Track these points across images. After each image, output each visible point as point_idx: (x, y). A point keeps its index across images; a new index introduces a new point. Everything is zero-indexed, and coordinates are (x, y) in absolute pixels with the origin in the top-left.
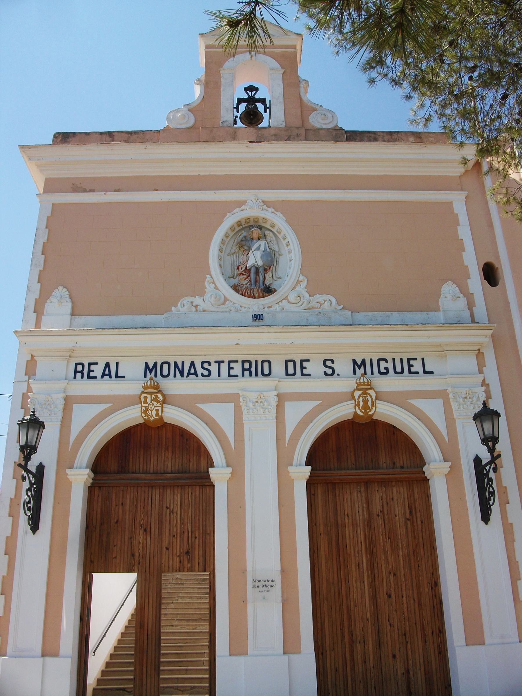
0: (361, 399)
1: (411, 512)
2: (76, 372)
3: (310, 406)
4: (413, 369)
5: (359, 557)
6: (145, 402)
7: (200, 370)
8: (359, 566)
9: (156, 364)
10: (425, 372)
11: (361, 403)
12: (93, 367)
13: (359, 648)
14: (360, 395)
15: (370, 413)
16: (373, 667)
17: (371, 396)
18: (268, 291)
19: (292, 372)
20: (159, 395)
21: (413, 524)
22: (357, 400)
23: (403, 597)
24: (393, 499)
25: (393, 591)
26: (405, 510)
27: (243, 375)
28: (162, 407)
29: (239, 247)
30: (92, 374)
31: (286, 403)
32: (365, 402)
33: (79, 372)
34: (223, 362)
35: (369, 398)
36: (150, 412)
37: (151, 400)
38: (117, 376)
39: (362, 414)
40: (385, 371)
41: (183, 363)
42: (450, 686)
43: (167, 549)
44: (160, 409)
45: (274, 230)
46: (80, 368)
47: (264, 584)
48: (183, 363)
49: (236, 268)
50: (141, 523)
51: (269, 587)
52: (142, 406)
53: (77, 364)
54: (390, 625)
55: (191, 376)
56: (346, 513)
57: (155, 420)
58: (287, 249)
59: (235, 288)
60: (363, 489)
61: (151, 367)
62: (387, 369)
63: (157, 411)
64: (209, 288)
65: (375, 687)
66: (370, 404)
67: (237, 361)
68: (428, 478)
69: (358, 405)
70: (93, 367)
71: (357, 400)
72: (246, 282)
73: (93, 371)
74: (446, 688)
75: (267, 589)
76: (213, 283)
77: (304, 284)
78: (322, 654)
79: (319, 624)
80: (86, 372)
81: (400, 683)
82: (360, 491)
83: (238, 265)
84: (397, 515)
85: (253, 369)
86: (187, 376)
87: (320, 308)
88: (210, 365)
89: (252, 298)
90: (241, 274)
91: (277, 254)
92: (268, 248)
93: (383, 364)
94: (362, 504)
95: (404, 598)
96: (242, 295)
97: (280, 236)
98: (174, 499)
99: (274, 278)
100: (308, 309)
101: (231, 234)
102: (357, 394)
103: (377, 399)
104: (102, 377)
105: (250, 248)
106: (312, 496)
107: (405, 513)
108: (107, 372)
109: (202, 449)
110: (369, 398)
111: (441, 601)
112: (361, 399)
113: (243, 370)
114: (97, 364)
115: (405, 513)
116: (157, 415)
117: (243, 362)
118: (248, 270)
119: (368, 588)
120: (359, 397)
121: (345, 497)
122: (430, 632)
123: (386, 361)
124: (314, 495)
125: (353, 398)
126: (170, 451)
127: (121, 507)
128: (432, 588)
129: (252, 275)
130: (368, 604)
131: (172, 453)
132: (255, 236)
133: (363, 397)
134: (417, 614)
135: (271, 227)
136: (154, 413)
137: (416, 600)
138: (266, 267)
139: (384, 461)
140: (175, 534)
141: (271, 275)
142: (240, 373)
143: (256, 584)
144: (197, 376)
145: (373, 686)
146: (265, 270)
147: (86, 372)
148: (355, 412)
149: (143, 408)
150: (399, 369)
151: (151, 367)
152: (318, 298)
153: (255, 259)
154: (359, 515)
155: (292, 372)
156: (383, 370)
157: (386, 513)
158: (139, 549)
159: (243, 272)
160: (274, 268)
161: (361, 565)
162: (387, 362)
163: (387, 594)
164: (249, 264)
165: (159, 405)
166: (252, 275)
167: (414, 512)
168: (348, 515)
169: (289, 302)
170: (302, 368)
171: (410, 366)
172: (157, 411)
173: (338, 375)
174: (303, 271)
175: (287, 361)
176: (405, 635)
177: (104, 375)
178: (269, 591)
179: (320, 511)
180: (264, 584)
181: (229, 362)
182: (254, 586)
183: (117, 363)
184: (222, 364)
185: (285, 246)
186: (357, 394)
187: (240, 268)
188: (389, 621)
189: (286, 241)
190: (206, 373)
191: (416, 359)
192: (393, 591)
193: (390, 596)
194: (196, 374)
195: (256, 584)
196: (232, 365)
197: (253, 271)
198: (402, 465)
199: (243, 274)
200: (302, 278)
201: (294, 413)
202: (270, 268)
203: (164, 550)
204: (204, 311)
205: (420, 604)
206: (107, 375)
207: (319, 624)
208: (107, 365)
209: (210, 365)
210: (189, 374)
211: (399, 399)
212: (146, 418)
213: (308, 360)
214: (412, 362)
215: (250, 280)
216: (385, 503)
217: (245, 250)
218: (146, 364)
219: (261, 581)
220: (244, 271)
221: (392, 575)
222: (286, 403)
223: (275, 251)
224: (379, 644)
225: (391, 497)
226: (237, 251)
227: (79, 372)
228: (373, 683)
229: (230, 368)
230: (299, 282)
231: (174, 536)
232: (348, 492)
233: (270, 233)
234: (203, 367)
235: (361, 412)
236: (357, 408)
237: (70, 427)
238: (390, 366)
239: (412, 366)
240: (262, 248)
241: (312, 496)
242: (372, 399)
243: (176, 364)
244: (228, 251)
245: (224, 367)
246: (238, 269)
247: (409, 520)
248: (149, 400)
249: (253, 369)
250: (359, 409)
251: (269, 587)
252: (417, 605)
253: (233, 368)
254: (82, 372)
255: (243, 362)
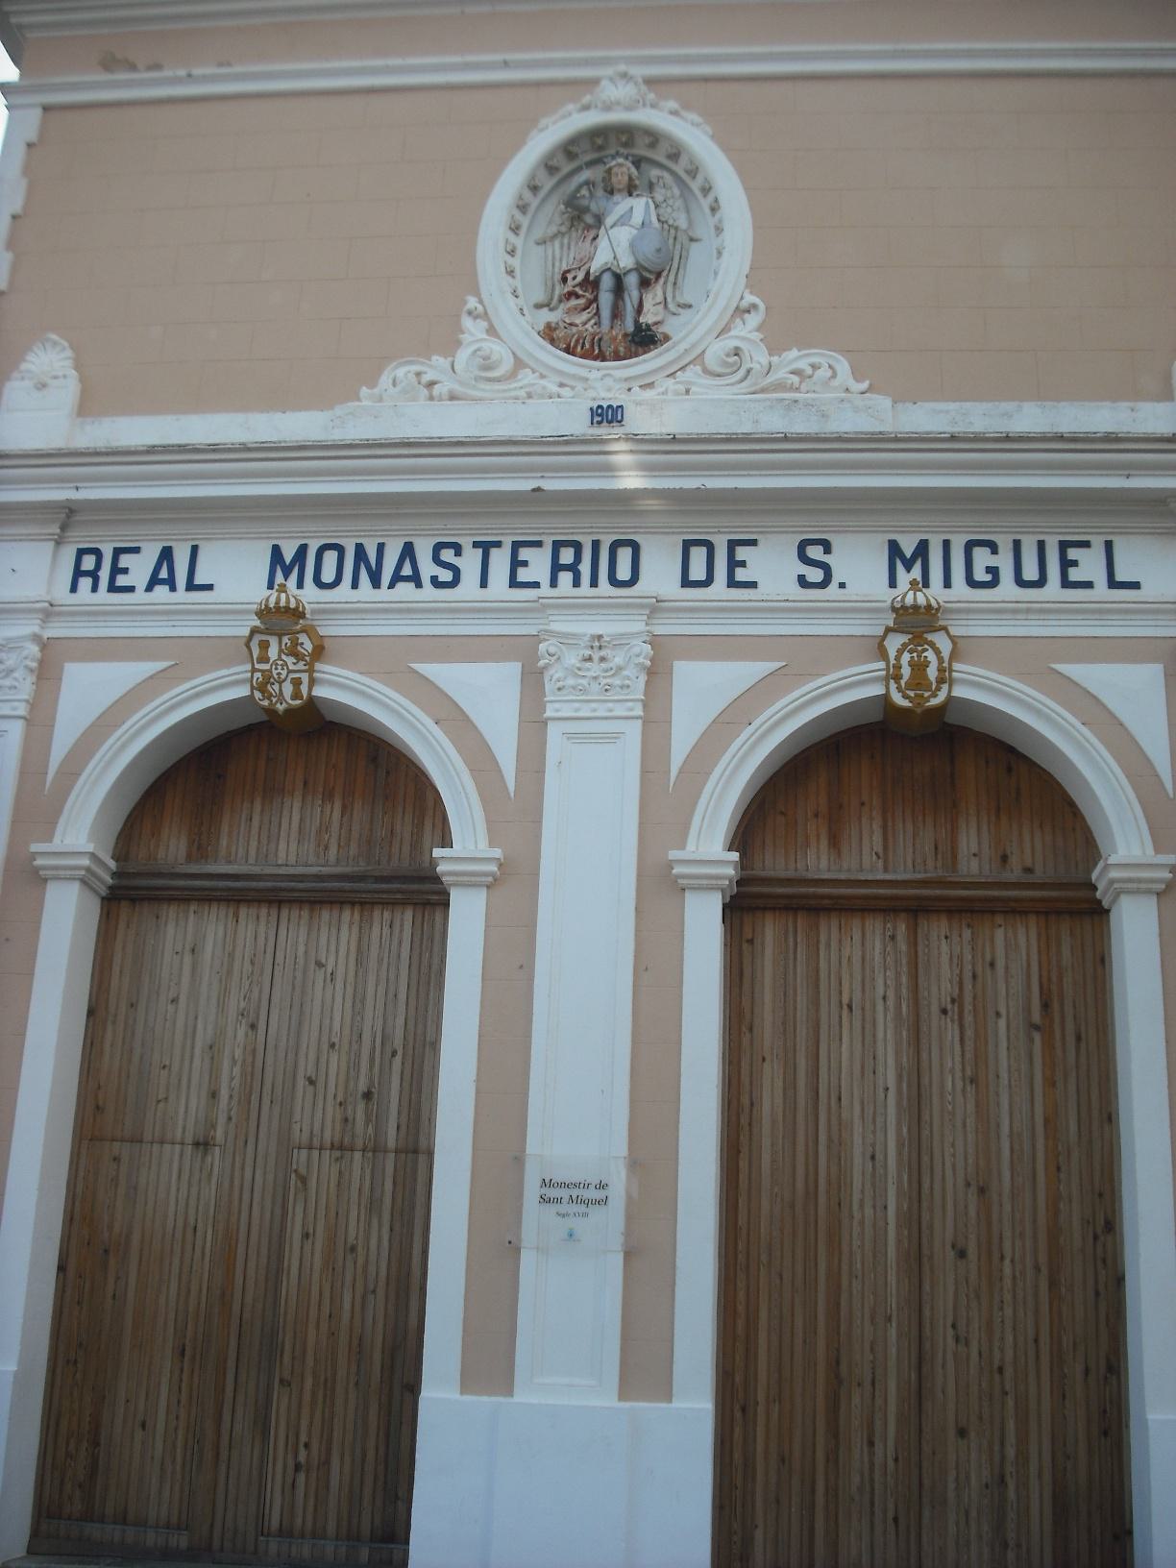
0: (906, 657)
1: (1046, 1006)
2: (78, 573)
3: (749, 672)
4: (1074, 574)
5: (874, 1132)
6: (264, 659)
7: (428, 569)
8: (873, 1158)
9: (302, 550)
10: (1113, 584)
11: (906, 671)
12: (125, 561)
13: (856, 1400)
14: (905, 645)
15: (934, 702)
16: (896, 1460)
17: (937, 652)
18: (644, 339)
19: (703, 577)
20: (303, 638)
21: (1048, 1045)
22: (892, 661)
23: (1002, 1258)
24: (992, 965)
25: (972, 1237)
26: (1028, 999)
27: (554, 583)
28: (311, 671)
29: (572, 219)
30: (122, 581)
31: (676, 664)
32: (919, 667)
33: (87, 573)
34: (498, 544)
35: (930, 655)
36: (276, 687)
37: (281, 651)
38: (191, 586)
39: (906, 703)
40: (988, 578)
41: (381, 548)
42: (1130, 1533)
43: (312, 1082)
44: (305, 677)
45: (679, 169)
46: (88, 562)
47: (575, 1193)
48: (381, 548)
49: (558, 277)
50: (243, 1004)
51: (587, 1203)
52: (254, 670)
53: (81, 553)
54: (957, 1340)
55: (400, 586)
56: (845, 1001)
57: (289, 711)
58: (712, 221)
59: (549, 334)
60: (902, 928)
61: (288, 560)
62: (993, 571)
63: (297, 683)
64: (473, 330)
65: (896, 1520)
66: (932, 673)
67: (538, 544)
68: (1105, 904)
69: (897, 678)
70: (125, 561)
71: (892, 661)
72: (585, 316)
73: (125, 571)
74: (1116, 1537)
75: (582, 1208)
76: (485, 316)
77: (843, 366)
78: (744, 1410)
79: (740, 1323)
80: (104, 574)
81: (973, 1514)
82: (893, 938)
83: (565, 267)
84: (1003, 1011)
85: (585, 568)
86: (391, 586)
87: (797, 390)
88: (458, 553)
89: (595, 359)
90: (571, 295)
91: (682, 238)
92: (654, 219)
93: (982, 558)
94: (898, 975)
95: (1007, 1262)
96: (567, 350)
97: (695, 186)
98: (336, 938)
99: (671, 306)
100: (763, 391)
101: (548, 183)
102: (894, 643)
103: (954, 655)
104: (149, 588)
105: (599, 220)
106: (745, 946)
107: (1028, 1010)
108: (164, 574)
109: (430, 803)
110: (930, 655)
111: (1120, 1280)
112: (906, 657)
113: (556, 568)
114: (136, 550)
115: (1028, 1010)
116: (296, 695)
117: (557, 545)
118: (591, 283)
119: (898, 1226)
120: (900, 652)
121: (846, 953)
122: (1079, 1368)
123: (994, 548)
124: (751, 941)
125: (883, 653)
126: (338, 805)
127: (188, 959)
128: (1096, 1238)
129: (606, 299)
130: (892, 1279)
131: (344, 808)
132: (620, 179)
133: (911, 652)
134: (1045, 1308)
135: (687, 172)
136: (288, 689)
137: (1044, 1270)
138: (647, 275)
139: (974, 849)
140: (336, 1040)
141: (660, 298)
142: (544, 578)
143: (552, 1193)
144: (419, 585)
145: (891, 1515)
146: (645, 284)
147: (104, 574)
148: (886, 697)
149: (258, 675)
150: (1030, 573)
151: (288, 560)
152: (794, 358)
153: (616, 245)
154: (886, 1009)
155: (703, 577)
156: (980, 575)
157: (968, 1007)
158: (232, 1079)
159: (577, 289)
160: (672, 278)
161: (879, 1156)
162: (995, 551)
163: (953, 1247)
164: (595, 267)
165: (301, 666)
166: (606, 299)
167: (1056, 1006)
168: (850, 1007)
169: (706, 371)
170: (733, 564)
171: (1066, 564)
172: (297, 683)
173: (842, 585)
174: (752, 282)
175: (687, 545)
176: (1001, 1370)
177: (154, 582)
178: (586, 1215)
179: (768, 998)
180: (575, 1193)
181: (516, 546)
182: (544, 1200)
183: (195, 549)
184: (494, 552)
185: (707, 211)
186: (894, 643)
187: (570, 276)
188: (954, 1326)
189: (711, 197)
190: (446, 576)
191: (1086, 544)
192: (972, 1237)
193: (962, 1254)
194: (416, 579)
195: (552, 1193)
196: (524, 554)
197: (607, 282)
198: (1028, 863)
199: (578, 296)
200: (750, 299)
201: (702, 689)
202: (659, 275)
203: (301, 1082)
204: (453, 397)
205: (1053, 1284)
206: (163, 582)
207: (740, 1323)
208: (167, 555)
209: (458, 553)
210: (397, 578)
211: (1036, 661)
212: (266, 703)
213: (753, 543)
214: (1073, 554)
215: (597, 313)
216: (967, 975)
217: (588, 227)
218: (276, 553)
219: (560, 1185)
220: (580, 285)
221: (973, 1189)
222: (676, 664)
223: (676, 228)
224: (919, 1394)
225: (988, 957)
226: (563, 229)
227: (87, 573)
228: (891, 1506)
229: (516, 564)
230: (741, 312)
231: (333, 1046)
232: (857, 937)
233: (666, 175)
234: (437, 560)
235: (905, 697)
236: (893, 685)
237: (50, 726)
238: (1004, 562)
239: (1075, 563)
240: (637, 218)
241: (745, 946)
242: (941, 660)
243: (360, 550)
244: (539, 233)
245: (500, 560)
246: (564, 280)
247: (1037, 1028)
248: (273, 652)
249: (585, 568)
250: (899, 689)
251: (587, 1203)
252: (1044, 1285)
253: (525, 564)
254: (94, 575)
255: (557, 545)
